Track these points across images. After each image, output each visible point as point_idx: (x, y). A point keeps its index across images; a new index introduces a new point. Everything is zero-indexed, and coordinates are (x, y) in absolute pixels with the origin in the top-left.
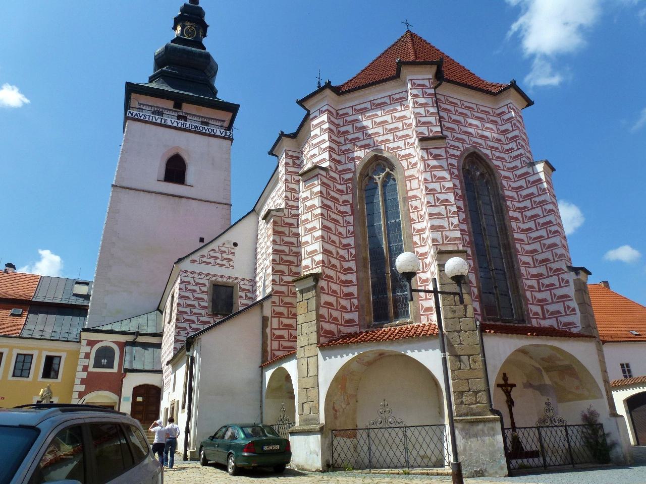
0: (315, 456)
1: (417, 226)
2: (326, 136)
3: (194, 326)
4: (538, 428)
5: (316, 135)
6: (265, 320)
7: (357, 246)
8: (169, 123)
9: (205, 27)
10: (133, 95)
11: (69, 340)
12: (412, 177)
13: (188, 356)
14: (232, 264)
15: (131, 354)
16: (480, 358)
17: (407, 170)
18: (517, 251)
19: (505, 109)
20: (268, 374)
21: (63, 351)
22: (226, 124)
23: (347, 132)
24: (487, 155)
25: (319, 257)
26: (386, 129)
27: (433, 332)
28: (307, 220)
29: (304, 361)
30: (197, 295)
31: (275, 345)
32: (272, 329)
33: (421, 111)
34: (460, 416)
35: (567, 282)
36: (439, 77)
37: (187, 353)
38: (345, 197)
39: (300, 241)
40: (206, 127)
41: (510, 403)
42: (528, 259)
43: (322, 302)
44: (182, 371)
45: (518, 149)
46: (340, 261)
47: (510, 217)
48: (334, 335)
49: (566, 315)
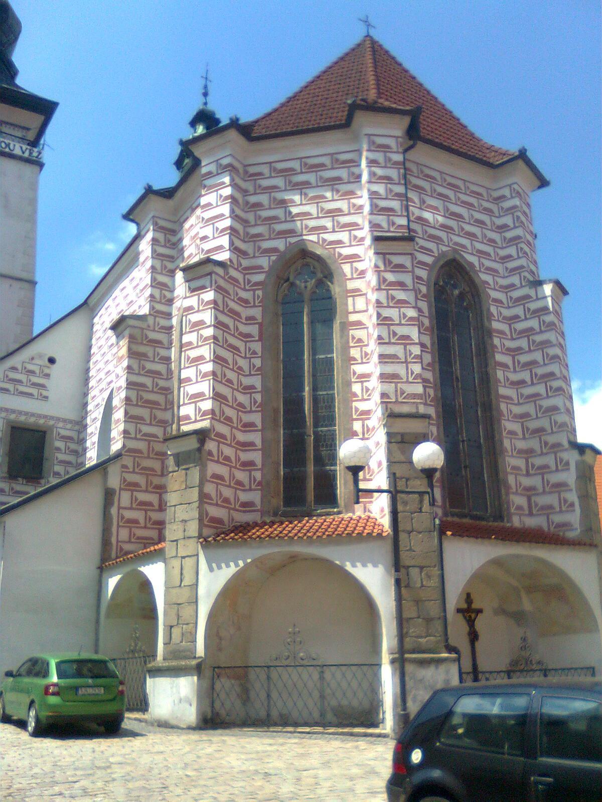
1: (359, 369)
2: (226, 209)
5: (209, 204)
6: (109, 496)
7: (265, 390)
12: (356, 293)
14: (45, 393)
16: (436, 571)
17: (350, 279)
18: (500, 413)
19: (506, 192)
20: (112, 582)
22: (31, 136)
23: (258, 205)
24: (472, 265)
25: (207, 405)
26: (322, 209)
27: (373, 531)
29: (176, 563)
31: (124, 534)
32: (119, 508)
33: (380, 188)
35: (567, 464)
36: (413, 134)
38: (251, 312)
39: (171, 370)
41: (474, 636)
42: (516, 427)
43: (209, 473)
45: (519, 258)
46: (238, 411)
47: (496, 362)
48: (224, 525)
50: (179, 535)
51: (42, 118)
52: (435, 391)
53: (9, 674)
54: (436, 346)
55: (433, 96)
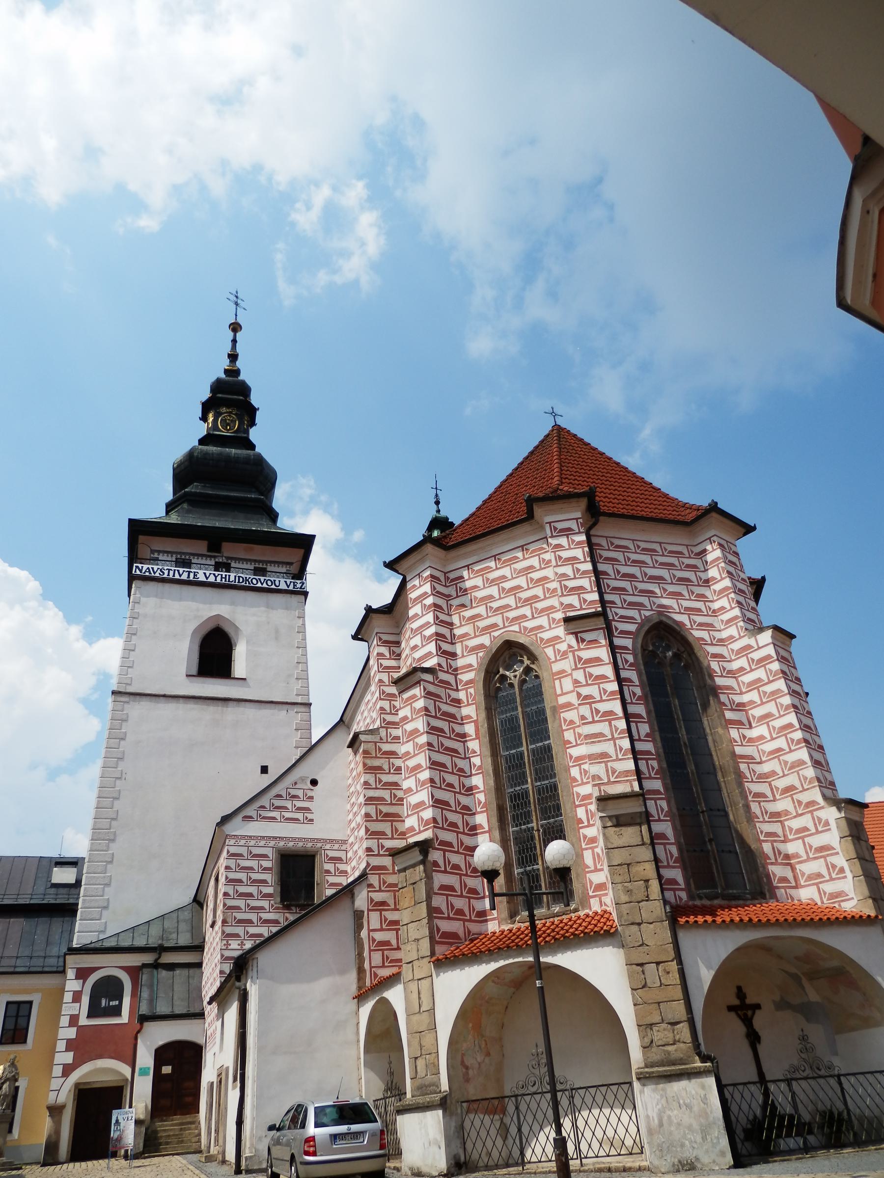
0: (436, 1149)
3: (252, 930)
4: (788, 1082)
5: (416, 615)
8: (202, 578)
9: (251, 411)
10: (141, 538)
11: (46, 969)
12: (562, 673)
13: (239, 988)
14: (310, 816)
15: (151, 986)
16: (674, 966)
21: (37, 991)
22: (294, 569)
24: (681, 624)
25: (428, 814)
28: (408, 753)
30: (255, 876)
31: (377, 958)
32: (370, 931)
34: (652, 1067)
35: (827, 823)
36: (594, 514)
37: (237, 984)
40: (262, 579)
44: (232, 1014)
46: (463, 814)
49: (832, 879)
50: (413, 956)
51: (302, 551)
52: (659, 764)
53: (272, 1128)
54: (653, 714)
55: (623, 467)
